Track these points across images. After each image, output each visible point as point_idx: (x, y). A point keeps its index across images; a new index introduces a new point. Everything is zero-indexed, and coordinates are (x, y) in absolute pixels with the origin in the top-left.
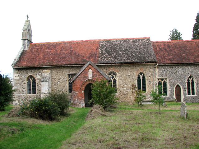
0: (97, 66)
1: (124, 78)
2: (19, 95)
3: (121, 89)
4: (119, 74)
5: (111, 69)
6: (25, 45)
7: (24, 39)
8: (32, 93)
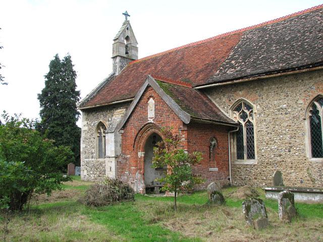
0: (199, 90)
1: (268, 119)
2: (87, 160)
3: (264, 148)
4: (258, 107)
5: (241, 95)
6: (116, 66)
7: (115, 55)
8: (245, 156)
